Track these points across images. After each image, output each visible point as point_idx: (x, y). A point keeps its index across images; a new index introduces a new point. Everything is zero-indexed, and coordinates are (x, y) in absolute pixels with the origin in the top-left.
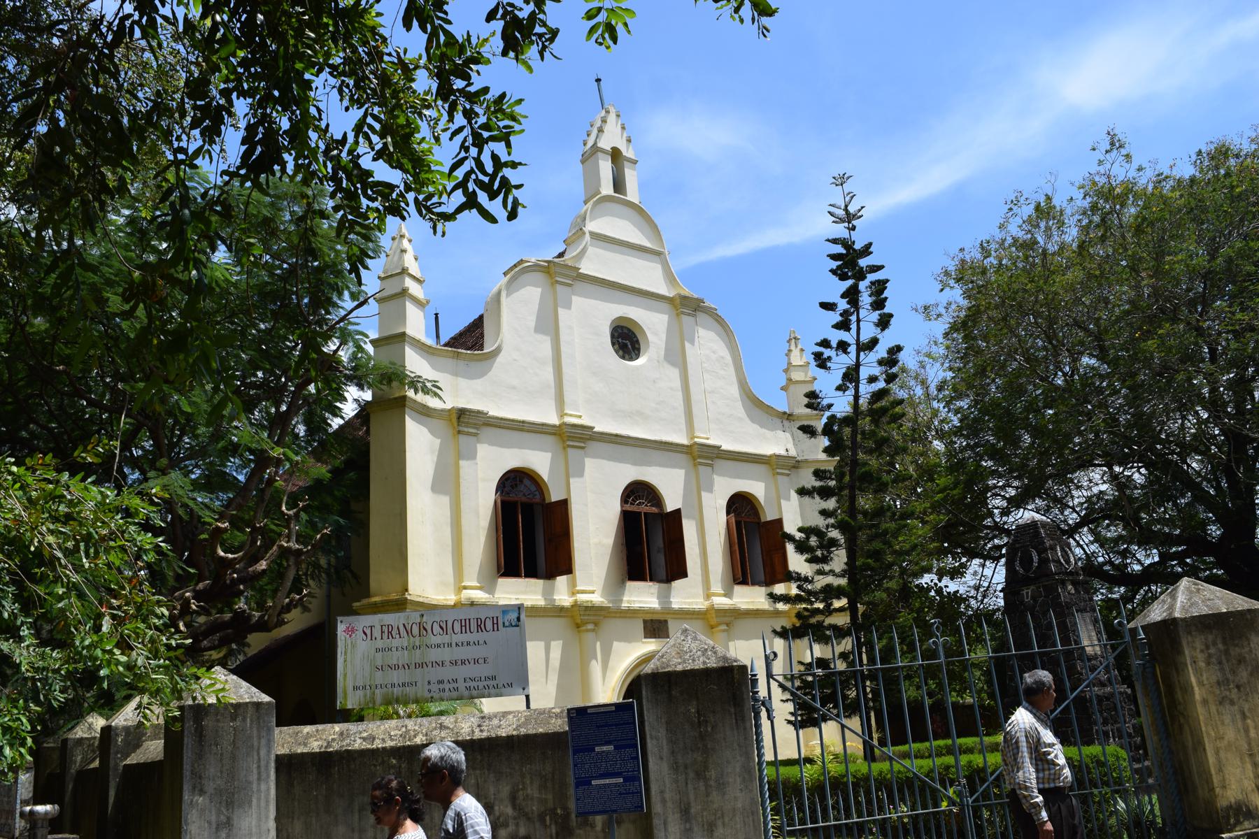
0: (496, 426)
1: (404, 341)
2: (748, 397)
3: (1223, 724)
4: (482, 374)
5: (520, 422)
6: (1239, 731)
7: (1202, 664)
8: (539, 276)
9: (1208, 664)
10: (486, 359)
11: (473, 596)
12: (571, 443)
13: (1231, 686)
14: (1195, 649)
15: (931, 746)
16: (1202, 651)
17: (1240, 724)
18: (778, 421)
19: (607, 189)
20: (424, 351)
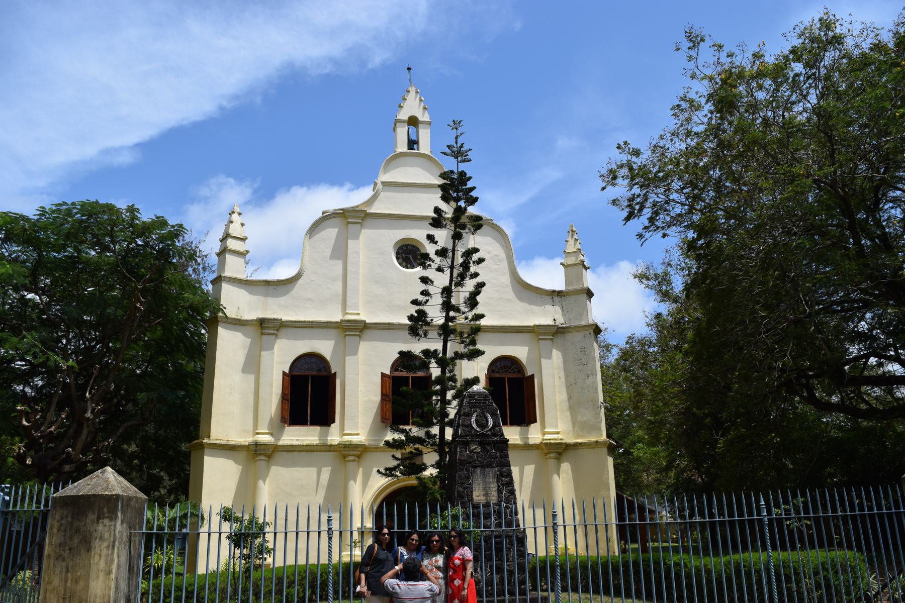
0: (293, 327)
1: (221, 280)
2: (518, 283)
3: (54, 573)
5: (310, 322)
6: (62, 580)
7: (55, 530)
8: (337, 221)
9: (59, 530)
11: (260, 439)
12: (348, 333)
13: (67, 548)
14: (54, 519)
15: (845, 555)
16: (58, 521)
17: (64, 574)
18: (549, 298)
19: (402, 147)
20: (243, 284)
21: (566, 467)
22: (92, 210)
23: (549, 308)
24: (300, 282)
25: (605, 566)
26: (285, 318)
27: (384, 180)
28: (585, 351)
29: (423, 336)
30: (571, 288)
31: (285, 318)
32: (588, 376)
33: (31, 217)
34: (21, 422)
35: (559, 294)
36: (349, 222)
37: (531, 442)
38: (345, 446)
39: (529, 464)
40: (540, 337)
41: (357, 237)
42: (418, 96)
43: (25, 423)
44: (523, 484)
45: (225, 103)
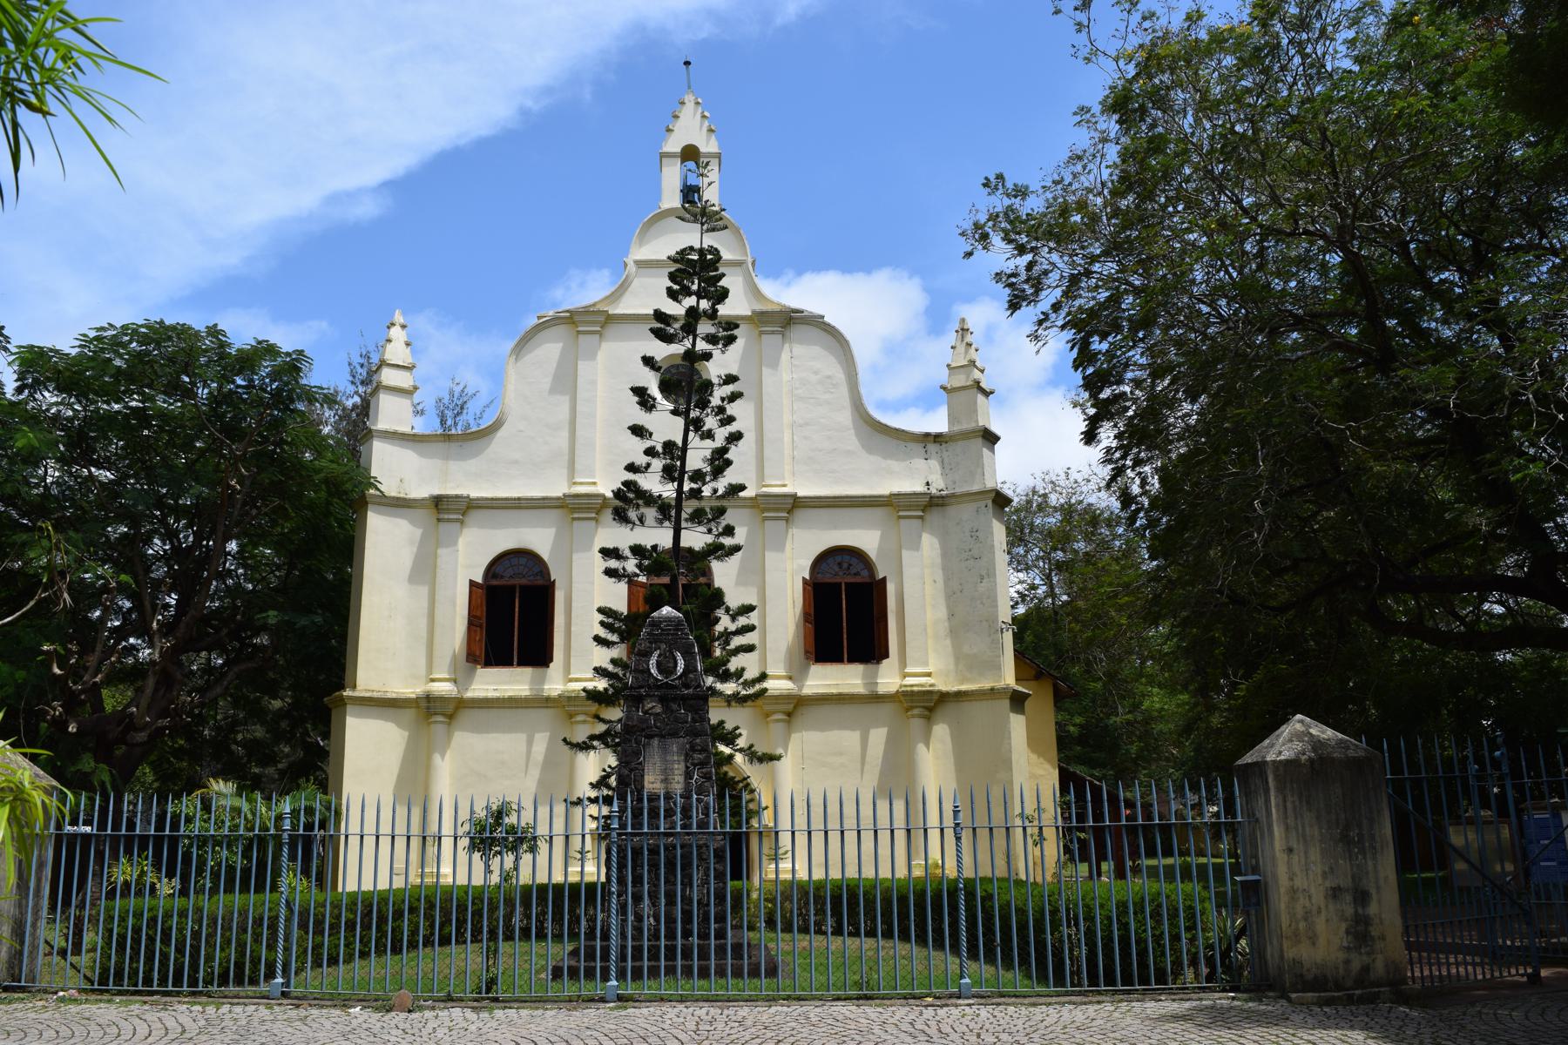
2: (866, 422)
4: (477, 454)
8: (561, 330)
10: (484, 436)
12: (576, 515)
18: (918, 448)
21: (941, 731)
22: (158, 333)
23: (919, 463)
24: (501, 433)
25: (920, 896)
26: (474, 494)
27: (639, 257)
28: (978, 536)
29: (638, 522)
30: (957, 428)
31: (475, 493)
32: (982, 578)
33: (67, 350)
34: (50, 669)
35: (937, 438)
36: (579, 332)
37: (881, 690)
38: (569, 698)
39: (877, 727)
40: (901, 513)
41: (592, 356)
42: (700, 110)
43: (57, 671)
44: (867, 759)
45: (529, 103)
